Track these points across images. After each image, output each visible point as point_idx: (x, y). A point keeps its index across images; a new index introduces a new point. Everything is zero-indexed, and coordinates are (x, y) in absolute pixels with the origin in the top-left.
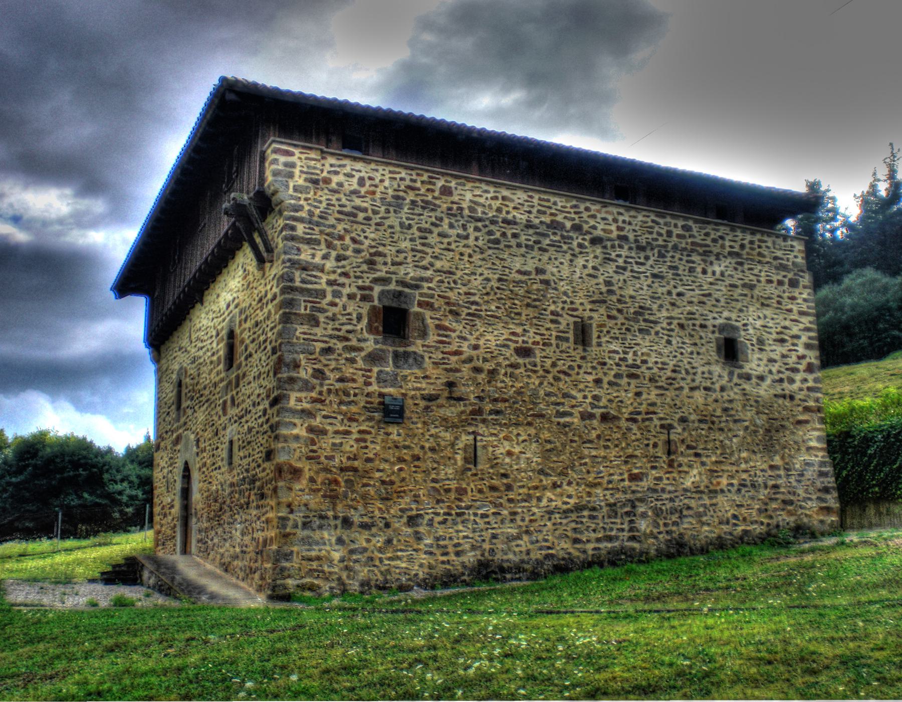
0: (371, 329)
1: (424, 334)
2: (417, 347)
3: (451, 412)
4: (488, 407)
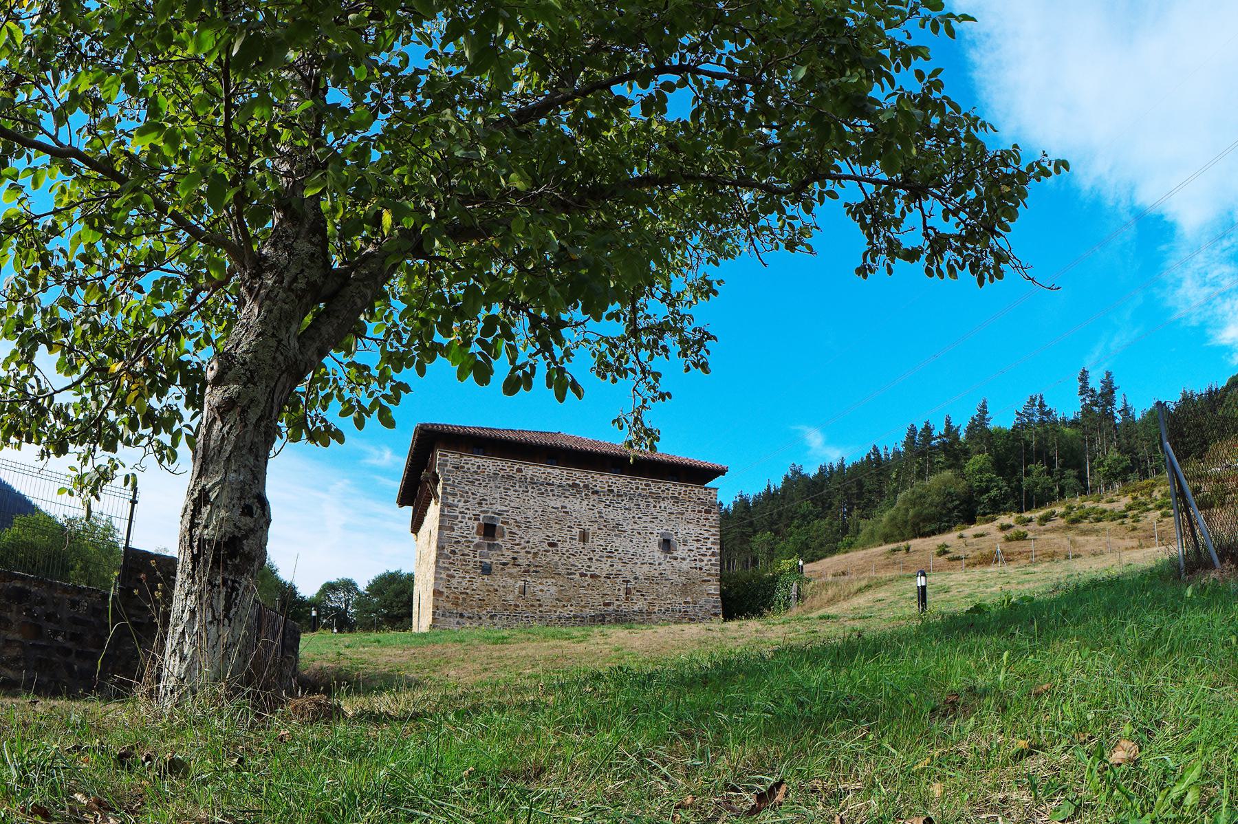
0: (478, 533)
1: (503, 536)
2: (499, 541)
3: (514, 570)
4: (532, 569)
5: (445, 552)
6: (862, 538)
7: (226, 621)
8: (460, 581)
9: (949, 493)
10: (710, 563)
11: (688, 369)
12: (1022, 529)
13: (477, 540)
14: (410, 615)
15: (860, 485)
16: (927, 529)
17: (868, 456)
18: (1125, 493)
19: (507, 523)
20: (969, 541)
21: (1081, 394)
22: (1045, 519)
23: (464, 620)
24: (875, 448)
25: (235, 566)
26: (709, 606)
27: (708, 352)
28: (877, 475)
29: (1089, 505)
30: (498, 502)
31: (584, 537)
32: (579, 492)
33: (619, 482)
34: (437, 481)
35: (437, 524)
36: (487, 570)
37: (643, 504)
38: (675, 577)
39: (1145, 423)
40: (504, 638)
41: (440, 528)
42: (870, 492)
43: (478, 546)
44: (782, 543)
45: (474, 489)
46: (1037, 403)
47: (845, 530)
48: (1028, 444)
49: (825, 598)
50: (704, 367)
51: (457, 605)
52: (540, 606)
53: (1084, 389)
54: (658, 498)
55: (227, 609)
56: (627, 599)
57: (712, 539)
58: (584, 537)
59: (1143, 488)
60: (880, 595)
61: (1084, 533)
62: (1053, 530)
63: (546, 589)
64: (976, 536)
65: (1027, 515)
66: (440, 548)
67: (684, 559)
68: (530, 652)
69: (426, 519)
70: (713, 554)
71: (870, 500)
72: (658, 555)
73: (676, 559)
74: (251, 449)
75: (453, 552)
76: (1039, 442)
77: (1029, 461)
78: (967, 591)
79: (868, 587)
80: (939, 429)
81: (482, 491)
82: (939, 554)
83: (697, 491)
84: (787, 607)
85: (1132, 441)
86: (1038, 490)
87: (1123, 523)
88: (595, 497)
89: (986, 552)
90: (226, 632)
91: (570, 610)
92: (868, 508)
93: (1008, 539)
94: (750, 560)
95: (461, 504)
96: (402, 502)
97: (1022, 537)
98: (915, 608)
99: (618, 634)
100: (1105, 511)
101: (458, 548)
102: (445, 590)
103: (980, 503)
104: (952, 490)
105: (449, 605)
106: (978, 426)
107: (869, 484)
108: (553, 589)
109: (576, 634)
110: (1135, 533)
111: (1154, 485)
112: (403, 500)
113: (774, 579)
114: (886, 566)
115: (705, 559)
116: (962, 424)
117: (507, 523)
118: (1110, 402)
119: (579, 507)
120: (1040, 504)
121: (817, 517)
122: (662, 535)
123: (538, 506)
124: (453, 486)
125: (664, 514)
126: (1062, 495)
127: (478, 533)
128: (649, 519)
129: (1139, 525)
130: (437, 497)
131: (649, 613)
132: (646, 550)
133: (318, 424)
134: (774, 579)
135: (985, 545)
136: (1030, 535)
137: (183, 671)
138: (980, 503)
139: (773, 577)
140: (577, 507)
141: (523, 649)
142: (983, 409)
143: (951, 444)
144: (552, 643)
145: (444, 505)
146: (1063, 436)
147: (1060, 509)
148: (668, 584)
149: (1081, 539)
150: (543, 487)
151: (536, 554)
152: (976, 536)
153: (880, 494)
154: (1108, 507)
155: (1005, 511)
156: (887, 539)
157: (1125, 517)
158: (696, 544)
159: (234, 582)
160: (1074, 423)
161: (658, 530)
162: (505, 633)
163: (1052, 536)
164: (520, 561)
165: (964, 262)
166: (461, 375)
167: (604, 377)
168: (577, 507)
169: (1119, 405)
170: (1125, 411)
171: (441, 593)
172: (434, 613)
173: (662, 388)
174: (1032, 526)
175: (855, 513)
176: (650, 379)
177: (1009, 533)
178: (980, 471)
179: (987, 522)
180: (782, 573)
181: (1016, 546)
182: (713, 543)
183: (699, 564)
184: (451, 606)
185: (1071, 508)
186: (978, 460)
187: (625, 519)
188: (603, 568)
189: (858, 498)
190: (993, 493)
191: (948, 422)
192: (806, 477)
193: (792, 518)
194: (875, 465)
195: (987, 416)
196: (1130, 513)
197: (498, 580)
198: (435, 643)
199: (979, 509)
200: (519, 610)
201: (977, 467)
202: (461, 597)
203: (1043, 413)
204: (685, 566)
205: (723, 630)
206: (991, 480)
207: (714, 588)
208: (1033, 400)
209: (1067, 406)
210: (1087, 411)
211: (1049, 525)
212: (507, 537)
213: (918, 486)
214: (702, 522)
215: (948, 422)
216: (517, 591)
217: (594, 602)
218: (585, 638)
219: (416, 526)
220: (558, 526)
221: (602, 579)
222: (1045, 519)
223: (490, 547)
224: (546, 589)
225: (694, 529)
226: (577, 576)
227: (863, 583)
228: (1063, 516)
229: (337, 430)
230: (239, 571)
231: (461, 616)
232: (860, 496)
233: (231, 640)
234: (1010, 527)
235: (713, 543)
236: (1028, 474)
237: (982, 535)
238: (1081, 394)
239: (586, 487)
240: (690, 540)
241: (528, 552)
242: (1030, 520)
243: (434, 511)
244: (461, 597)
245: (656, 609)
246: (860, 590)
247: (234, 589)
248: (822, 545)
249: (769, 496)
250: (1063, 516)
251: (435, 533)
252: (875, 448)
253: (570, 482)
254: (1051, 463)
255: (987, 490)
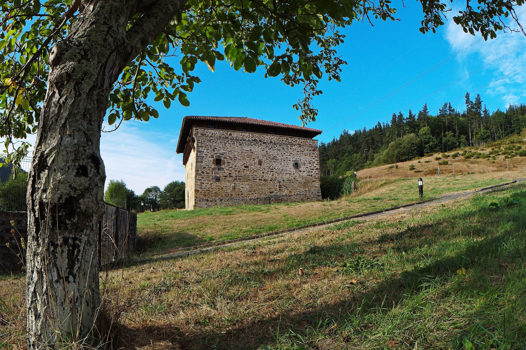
0: (213, 163)
1: (224, 164)
2: (223, 166)
3: (230, 179)
4: (238, 178)
5: (199, 172)
6: (375, 162)
7: (71, 278)
8: (206, 185)
9: (413, 143)
10: (316, 173)
11: (330, 79)
12: (446, 160)
13: (213, 166)
14: (184, 200)
15: (373, 139)
16: (403, 158)
17: (376, 127)
18: (489, 147)
19: (226, 158)
20: (423, 164)
21: (466, 103)
22: (455, 156)
23: (209, 202)
24: (379, 123)
25: (73, 224)
26: (315, 192)
27: (340, 70)
28: (380, 135)
29: (473, 151)
30: (221, 149)
31: (260, 163)
32: (257, 143)
33: (275, 138)
34: (194, 141)
35: (195, 160)
36: (218, 179)
37: (285, 148)
38: (300, 180)
39: (494, 117)
40: (230, 212)
41: (197, 162)
42: (377, 142)
43: (213, 169)
44: (340, 164)
45: (211, 144)
46: (448, 106)
47: (367, 158)
48: (444, 123)
49: (367, 188)
50: (337, 78)
51: (205, 196)
52: (242, 194)
53: (468, 101)
54: (292, 145)
55: (71, 266)
56: (280, 190)
57: (316, 162)
58: (260, 163)
59: (496, 145)
60: (392, 188)
61: (472, 163)
62: (459, 161)
63: (244, 187)
64: (426, 162)
65: (447, 154)
66: (197, 171)
67: (304, 171)
68: (244, 218)
69: (190, 158)
70: (317, 169)
71: (377, 145)
72: (293, 170)
73: (301, 171)
74: (84, 115)
75: (203, 172)
76: (449, 123)
77: (445, 131)
78: (431, 187)
79: (385, 184)
80: (406, 115)
81: (214, 144)
82: (411, 169)
83: (309, 142)
84: (350, 192)
85: (488, 125)
86: (450, 143)
87: (489, 160)
88: (265, 145)
89: (431, 169)
90: (72, 289)
91: (255, 196)
92: (376, 149)
93: (440, 164)
94: (327, 171)
95: (205, 151)
96: (179, 151)
97: (446, 163)
98: (418, 196)
99: (283, 208)
100: (481, 154)
101: (204, 170)
102: (200, 189)
103: (426, 148)
104: (414, 142)
105: (202, 196)
106: (423, 114)
107: (377, 138)
108: (248, 187)
109: (263, 208)
110: (494, 164)
111: (500, 144)
112: (179, 151)
113: (343, 180)
114: (388, 174)
115: (313, 171)
116: (416, 114)
117: (226, 158)
118: (479, 107)
119: (257, 150)
120: (451, 149)
121: (355, 152)
122: (294, 161)
123: (239, 150)
124: (201, 143)
125: (295, 151)
126: (459, 146)
127: (213, 163)
128: (288, 154)
129: (496, 161)
130: (194, 148)
131: (290, 196)
132: (288, 168)
133: (141, 108)
134: (343, 180)
135: (431, 166)
136: (449, 163)
137: (39, 328)
138: (426, 148)
139: (343, 179)
140: (257, 150)
141: (241, 217)
142: (425, 108)
143: (412, 122)
144: (253, 213)
145: (198, 151)
146: (459, 121)
147: (461, 152)
148: (297, 182)
149: (472, 165)
150: (241, 142)
151: (239, 171)
152: (426, 162)
153: (382, 143)
154: (482, 152)
155: (436, 152)
156: (386, 162)
157: (490, 157)
158: (309, 165)
159: (75, 239)
160: (464, 116)
161: (293, 159)
162: (230, 209)
163: (458, 163)
164: (232, 175)
165: (478, 27)
166: (237, 66)
167: (288, 83)
168: (257, 150)
169: (483, 109)
170: (485, 111)
171: (198, 191)
172: (195, 200)
173: (318, 89)
174: (449, 159)
175: (371, 151)
176: (312, 84)
177: (440, 161)
178: (425, 134)
179: (429, 156)
180: (347, 177)
181: (444, 167)
182: (317, 164)
183: (311, 174)
184: (202, 196)
185: (466, 152)
186: (424, 129)
187: (278, 154)
188: (269, 176)
189: (372, 145)
190: (431, 144)
191: (410, 113)
192: (349, 135)
193: (345, 153)
194: (379, 130)
195: (427, 111)
196: (491, 156)
197: (223, 184)
198: (199, 216)
199: (425, 151)
200: (233, 196)
201: (424, 132)
202: (207, 192)
203: (450, 110)
204: (305, 174)
205: (331, 205)
206: (429, 138)
207: (317, 184)
208: (446, 105)
209: (461, 108)
210: (469, 110)
211: (457, 159)
212: (226, 165)
213: (398, 140)
214: (312, 155)
215: (410, 113)
216: (231, 188)
217: (265, 192)
218: (268, 211)
219: (185, 162)
220: (249, 159)
221: (269, 182)
222: (455, 156)
223: (219, 169)
224: (244, 187)
225: (308, 158)
226: (258, 180)
227: (383, 182)
228: (462, 155)
229: (153, 110)
230: (78, 229)
231: (207, 200)
232: (373, 143)
233: (77, 294)
234: (440, 158)
235: (317, 164)
236: (445, 136)
237: (428, 162)
238: (466, 103)
239: (260, 141)
240: (306, 163)
241: (236, 171)
242: (449, 156)
243: (193, 155)
244: (207, 192)
245: (293, 194)
246: (382, 185)
247: (75, 246)
248: (357, 164)
249: (334, 143)
250: (462, 155)
251: (194, 165)
252: (379, 123)
253: (253, 139)
254: (454, 131)
255: (428, 142)
